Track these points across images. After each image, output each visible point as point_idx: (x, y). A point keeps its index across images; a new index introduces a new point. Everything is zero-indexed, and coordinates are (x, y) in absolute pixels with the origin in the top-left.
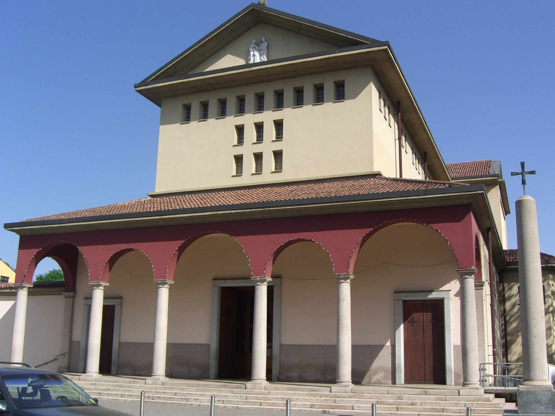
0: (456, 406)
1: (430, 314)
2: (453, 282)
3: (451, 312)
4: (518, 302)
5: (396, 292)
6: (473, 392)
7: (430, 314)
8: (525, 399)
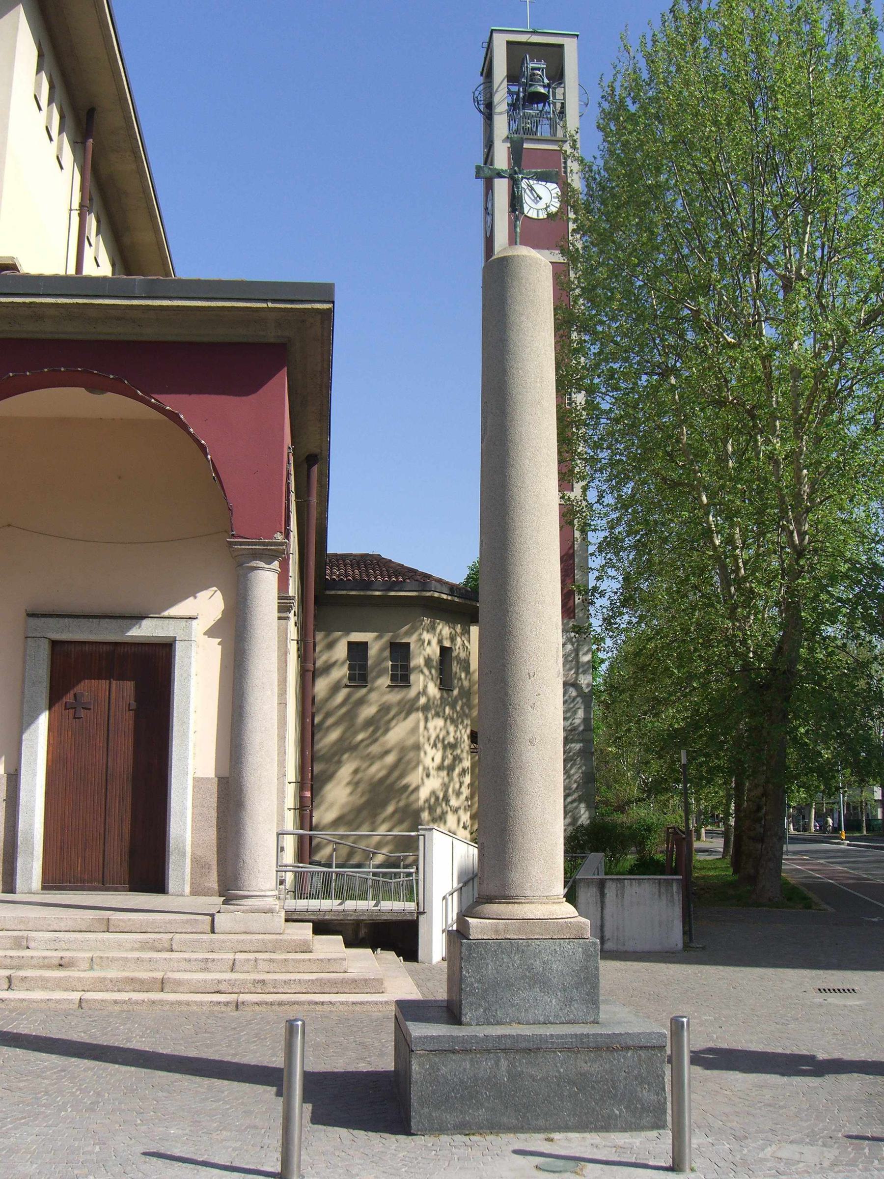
0: (205, 970)
1: (129, 686)
2: (203, 595)
3: (194, 681)
4: (346, 681)
5: (31, 615)
6: (257, 921)
7: (129, 686)
8: (490, 969)
